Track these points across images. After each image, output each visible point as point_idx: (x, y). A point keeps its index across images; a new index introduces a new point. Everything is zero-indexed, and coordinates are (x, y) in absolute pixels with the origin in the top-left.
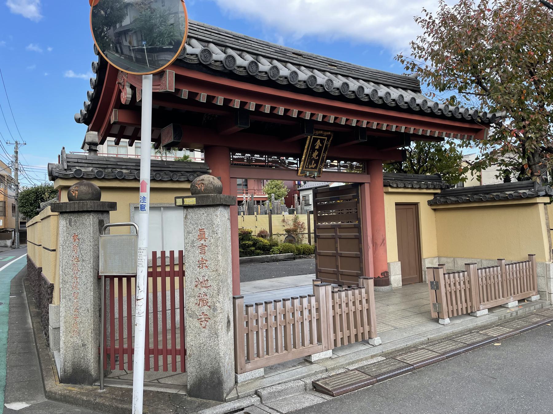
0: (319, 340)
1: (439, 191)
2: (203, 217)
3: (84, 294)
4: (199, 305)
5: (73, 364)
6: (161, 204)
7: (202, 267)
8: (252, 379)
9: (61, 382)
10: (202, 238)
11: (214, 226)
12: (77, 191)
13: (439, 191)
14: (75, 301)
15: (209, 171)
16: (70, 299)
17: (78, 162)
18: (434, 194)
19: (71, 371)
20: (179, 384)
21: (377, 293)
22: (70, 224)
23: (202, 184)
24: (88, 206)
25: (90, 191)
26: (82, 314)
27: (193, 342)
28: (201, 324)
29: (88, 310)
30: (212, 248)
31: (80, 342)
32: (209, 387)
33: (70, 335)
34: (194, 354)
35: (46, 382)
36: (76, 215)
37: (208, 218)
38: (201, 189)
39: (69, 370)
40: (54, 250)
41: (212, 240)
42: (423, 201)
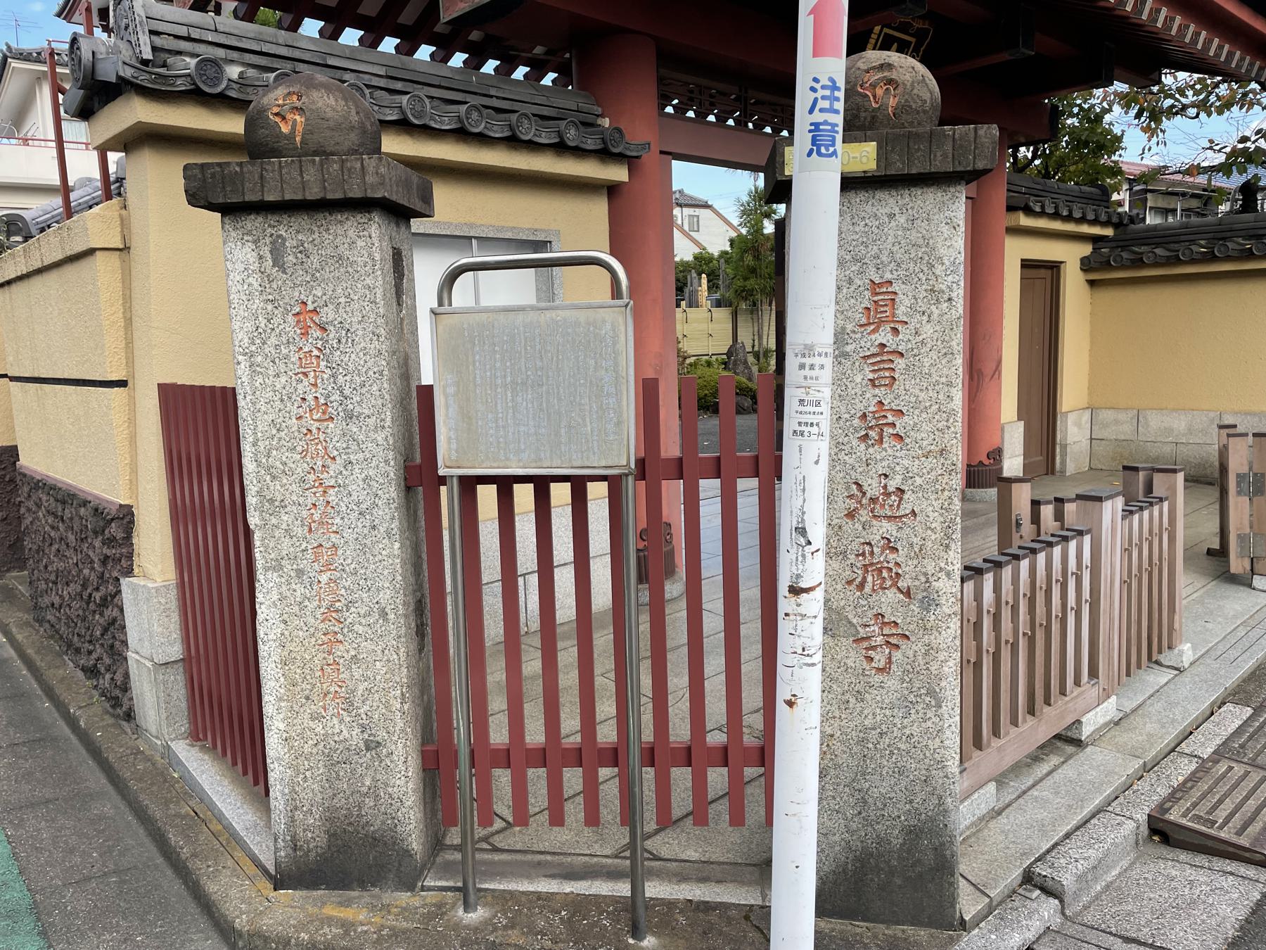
0: (1093, 673)
1: (1109, 232)
2: (891, 230)
3: (363, 549)
4: (861, 586)
5: (330, 817)
6: (471, 226)
7: (881, 441)
8: (973, 824)
9: (280, 881)
10: (881, 322)
11: (939, 270)
12: (300, 110)
13: (1109, 232)
14: (324, 578)
15: (600, 121)
16: (300, 573)
17: (188, 39)
18: (1095, 240)
19: (322, 840)
20: (730, 857)
21: (971, 506)
22: (278, 262)
23: (890, 81)
24: (370, 179)
25: (354, 118)
26: (360, 629)
27: (837, 723)
28: (870, 659)
29: (383, 614)
30: (927, 362)
31: (356, 738)
32: (898, 881)
33: (311, 708)
34: (837, 767)
35: (212, 887)
36: (302, 221)
37: (914, 236)
38: (882, 108)
39: (314, 835)
40: (122, 384)
41: (928, 330)
42: (1070, 255)
